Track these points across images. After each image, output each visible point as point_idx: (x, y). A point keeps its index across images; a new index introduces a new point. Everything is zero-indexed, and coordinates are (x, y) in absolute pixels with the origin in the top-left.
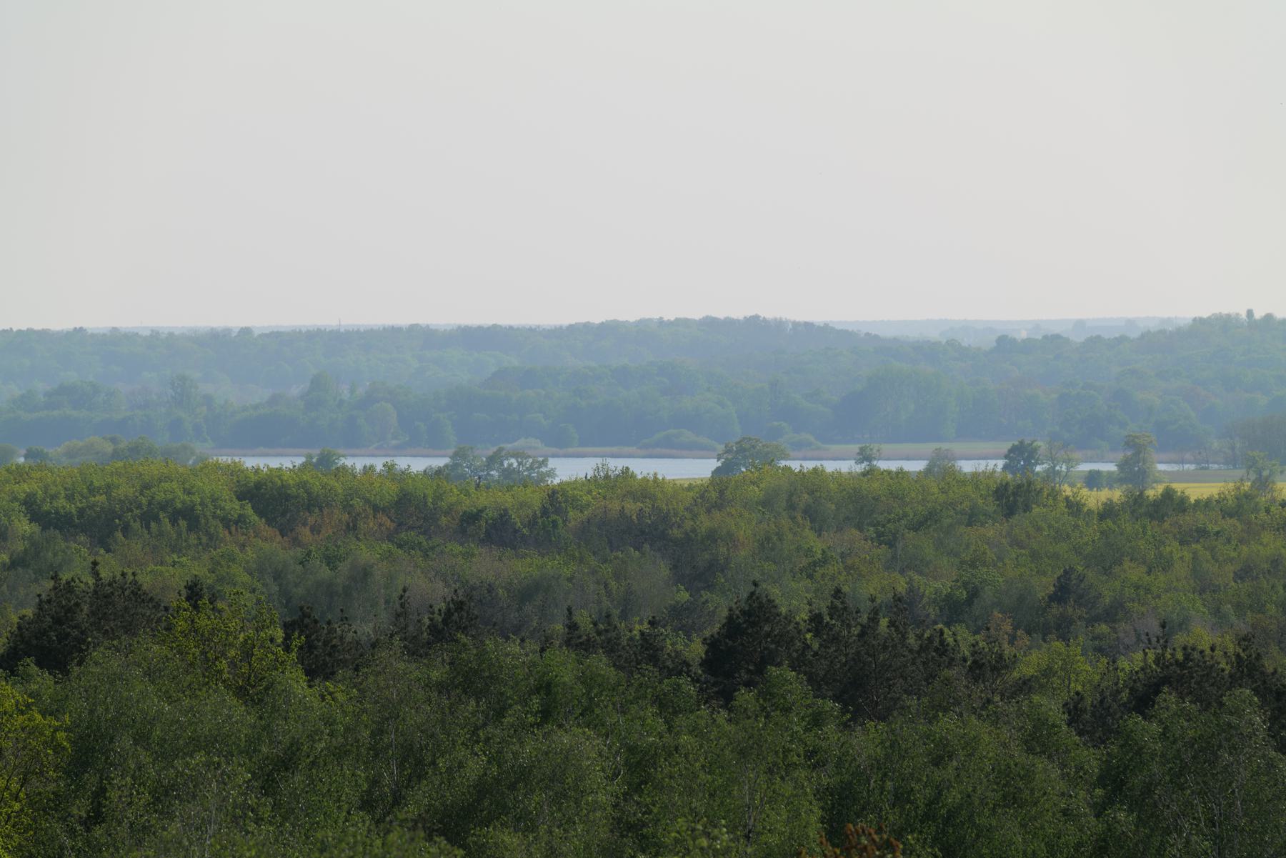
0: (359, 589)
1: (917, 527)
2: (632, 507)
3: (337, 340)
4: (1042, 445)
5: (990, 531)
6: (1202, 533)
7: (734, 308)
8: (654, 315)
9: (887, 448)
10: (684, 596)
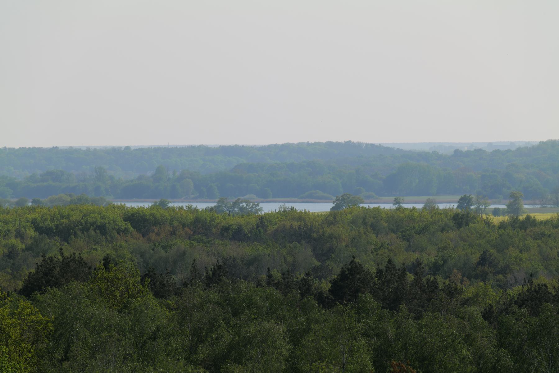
2: (296, 224)
9: (406, 198)
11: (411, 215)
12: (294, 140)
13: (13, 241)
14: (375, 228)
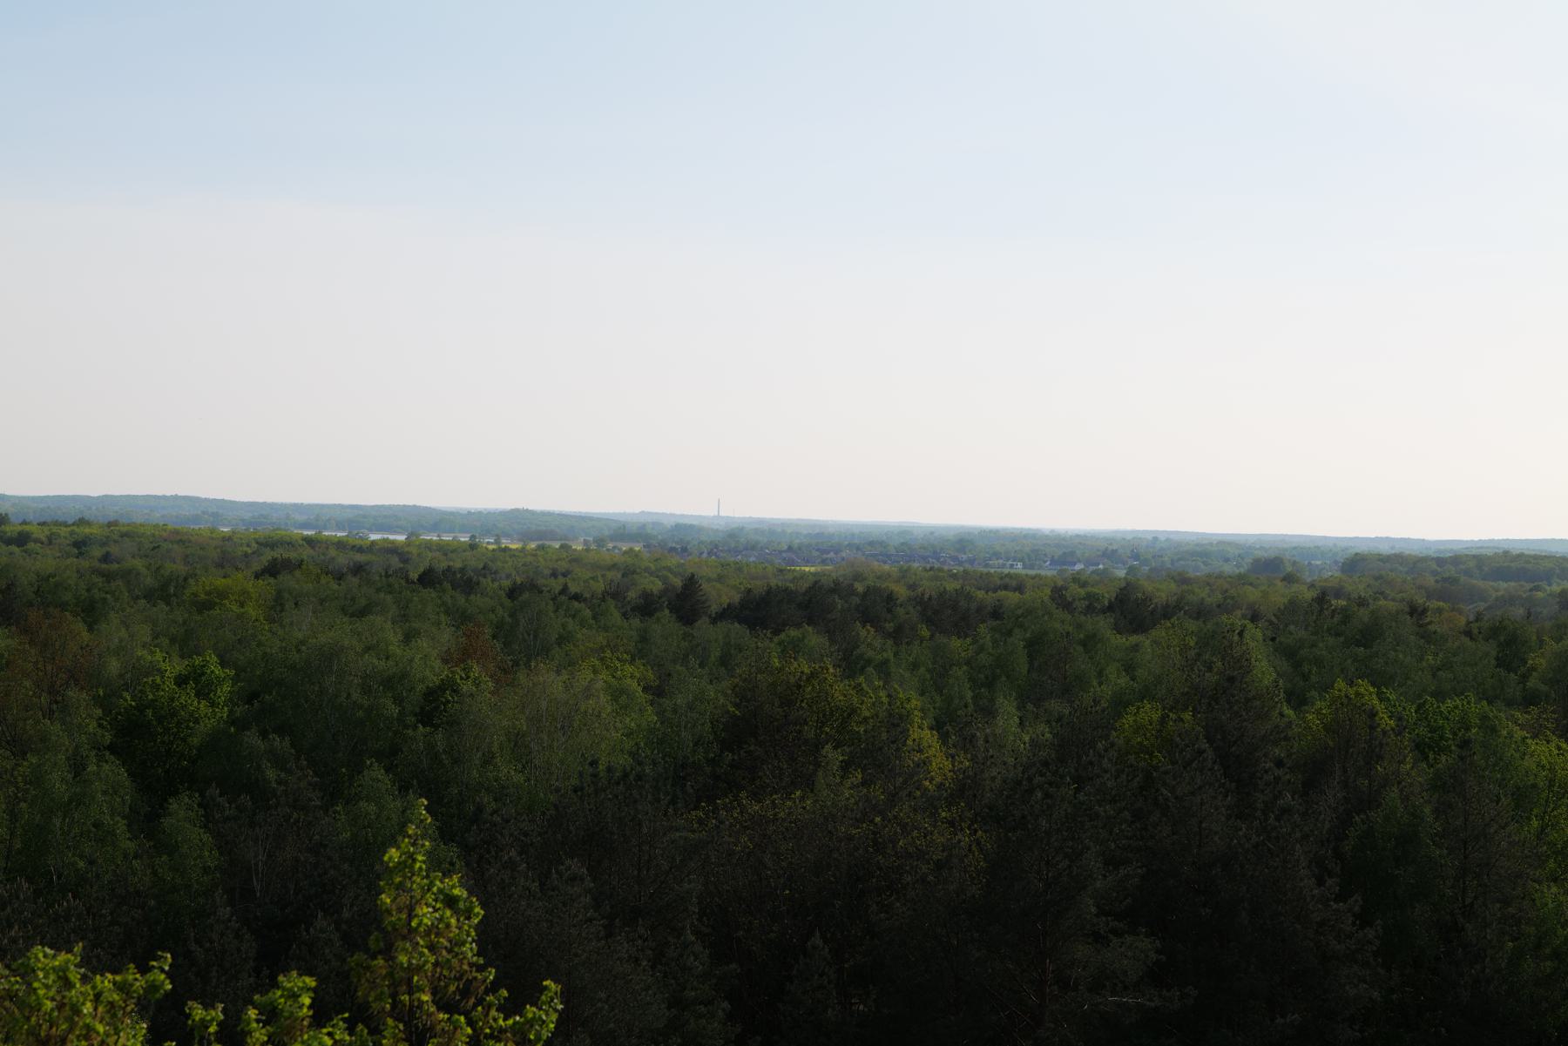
0: (1036, 589)
1: (452, 552)
2: (390, 545)
3: (322, 506)
4: (477, 535)
5: (468, 553)
6: (514, 555)
7: (410, 502)
8: (392, 503)
9: (445, 535)
10: (402, 565)
11: (448, 543)
12: (269, 500)
13: (245, 549)
14: (430, 549)
